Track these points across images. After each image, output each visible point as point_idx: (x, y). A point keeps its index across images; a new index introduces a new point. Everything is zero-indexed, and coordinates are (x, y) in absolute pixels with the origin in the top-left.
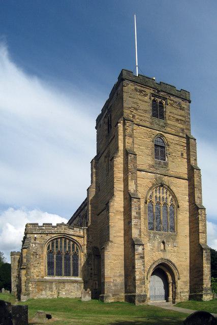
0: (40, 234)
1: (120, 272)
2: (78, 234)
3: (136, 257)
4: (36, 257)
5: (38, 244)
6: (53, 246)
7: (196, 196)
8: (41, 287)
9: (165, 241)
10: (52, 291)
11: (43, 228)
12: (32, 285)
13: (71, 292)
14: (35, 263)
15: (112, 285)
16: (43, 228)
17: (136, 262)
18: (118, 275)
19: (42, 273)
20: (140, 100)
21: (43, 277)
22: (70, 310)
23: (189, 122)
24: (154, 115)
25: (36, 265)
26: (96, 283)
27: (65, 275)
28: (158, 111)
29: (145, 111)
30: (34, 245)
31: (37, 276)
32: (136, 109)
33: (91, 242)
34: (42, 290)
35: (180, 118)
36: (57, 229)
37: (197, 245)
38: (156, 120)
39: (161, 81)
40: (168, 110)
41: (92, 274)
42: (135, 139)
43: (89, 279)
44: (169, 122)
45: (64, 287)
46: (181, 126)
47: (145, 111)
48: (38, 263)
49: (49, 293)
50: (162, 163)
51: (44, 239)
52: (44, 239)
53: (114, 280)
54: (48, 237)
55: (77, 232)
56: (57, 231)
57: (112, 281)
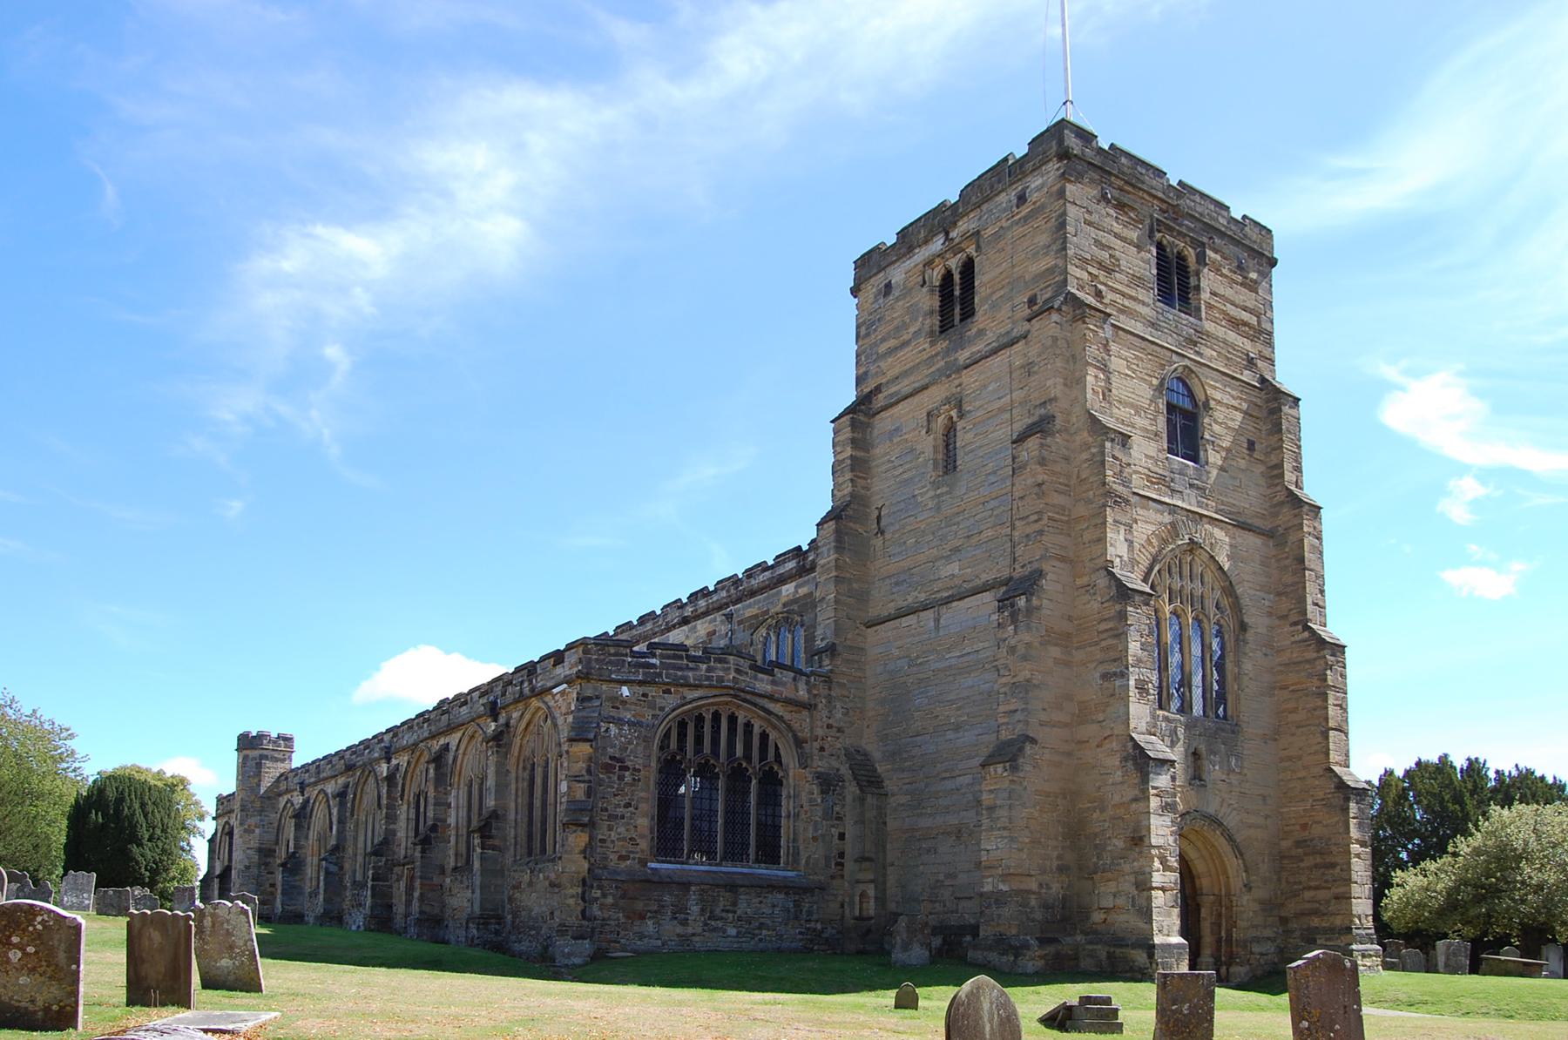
0: (641, 683)
1: (1059, 857)
2: (787, 692)
3: (1154, 803)
4: (621, 778)
5: (630, 724)
6: (682, 736)
7: (1309, 601)
8: (639, 906)
9: (1202, 748)
10: (684, 923)
11: (653, 661)
12: (604, 896)
13: (761, 926)
14: (615, 801)
15: (1033, 903)
16: (653, 661)
17: (1155, 821)
18: (1055, 863)
19: (644, 844)
20: (1117, 236)
21: (643, 863)
22: (1511, 1017)
23: (1270, 334)
24: (1165, 295)
25: (620, 811)
26: (863, 895)
27: (757, 861)
28: (1175, 281)
29: (1137, 281)
30: (614, 730)
31: (621, 858)
32: (1109, 271)
33: (840, 730)
34: (642, 917)
35: (1245, 316)
36: (709, 670)
37: (1318, 770)
38: (1173, 314)
39: (1119, 144)
40: (1209, 282)
41: (842, 855)
42: (1114, 379)
43: (833, 877)
44: (1209, 326)
45: (734, 904)
46: (1247, 345)
47: (1137, 281)
48: (628, 805)
49: (671, 929)
50: (1191, 472)
51: (652, 706)
52: (652, 706)
53: (1041, 885)
54: (671, 701)
55: (784, 684)
56: (708, 678)
57: (1034, 886)
